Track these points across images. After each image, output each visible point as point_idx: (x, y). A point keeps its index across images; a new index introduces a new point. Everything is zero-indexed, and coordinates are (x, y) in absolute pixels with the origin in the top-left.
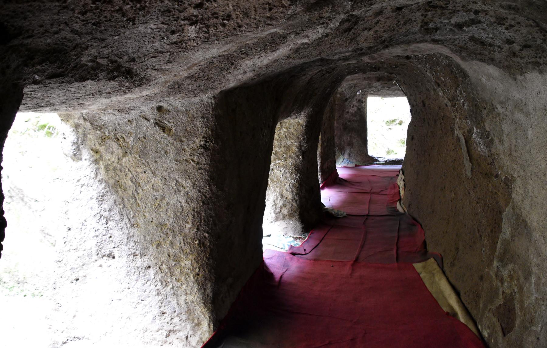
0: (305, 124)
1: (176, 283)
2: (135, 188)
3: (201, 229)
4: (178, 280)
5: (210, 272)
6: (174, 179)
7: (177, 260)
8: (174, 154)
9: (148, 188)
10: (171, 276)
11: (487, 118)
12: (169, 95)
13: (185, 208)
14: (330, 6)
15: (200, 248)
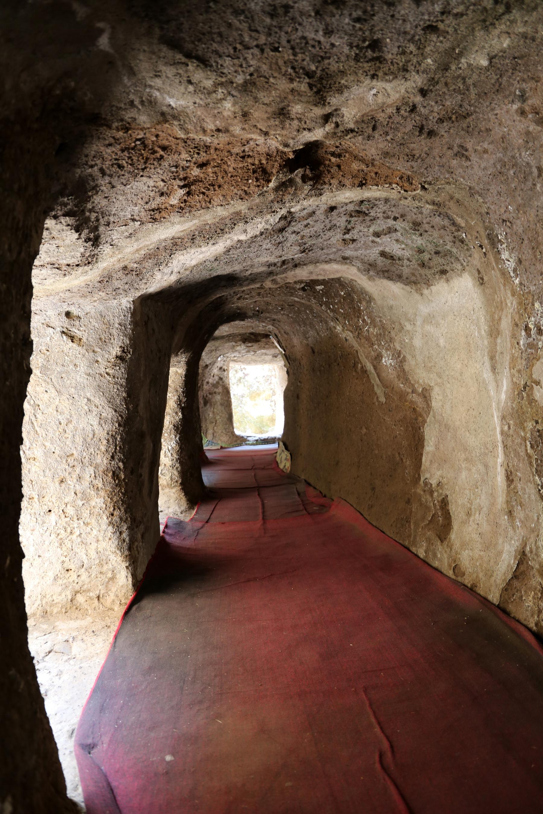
0: (184, 373)
1: (85, 527)
2: (33, 411)
3: (116, 457)
4: (86, 524)
5: (126, 512)
6: (84, 398)
7: (86, 498)
8: (86, 368)
9: (51, 410)
10: (78, 519)
11: (396, 338)
12: (83, 296)
13: (97, 432)
14: (294, 188)
15: (115, 481)
